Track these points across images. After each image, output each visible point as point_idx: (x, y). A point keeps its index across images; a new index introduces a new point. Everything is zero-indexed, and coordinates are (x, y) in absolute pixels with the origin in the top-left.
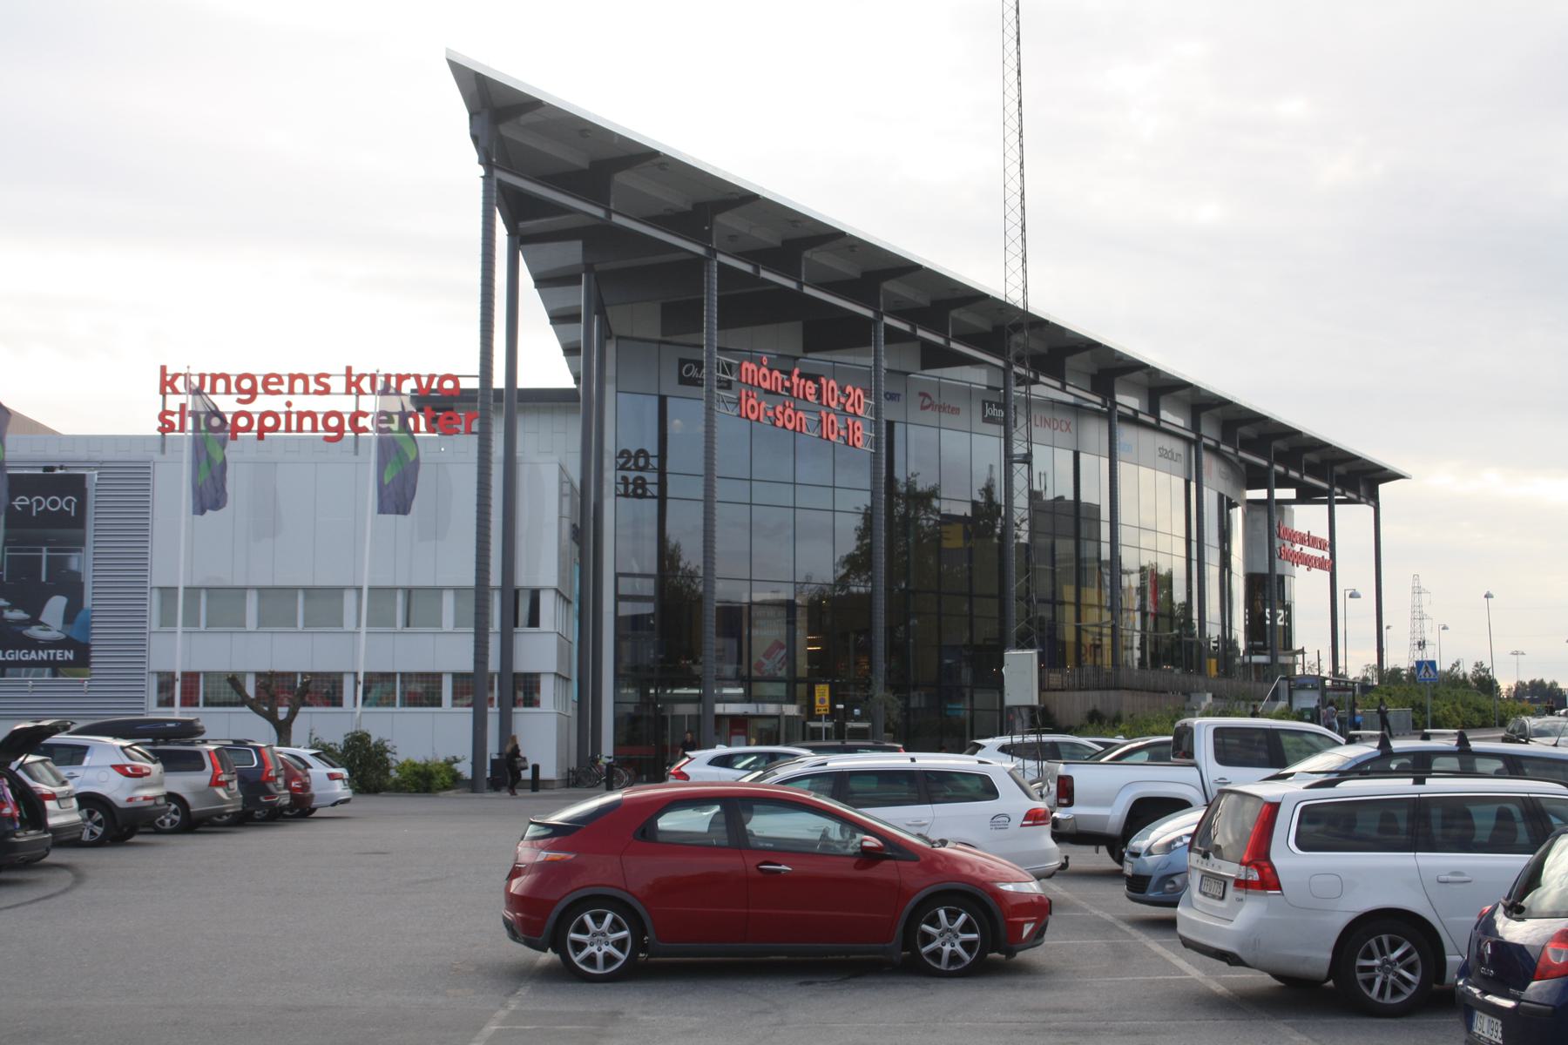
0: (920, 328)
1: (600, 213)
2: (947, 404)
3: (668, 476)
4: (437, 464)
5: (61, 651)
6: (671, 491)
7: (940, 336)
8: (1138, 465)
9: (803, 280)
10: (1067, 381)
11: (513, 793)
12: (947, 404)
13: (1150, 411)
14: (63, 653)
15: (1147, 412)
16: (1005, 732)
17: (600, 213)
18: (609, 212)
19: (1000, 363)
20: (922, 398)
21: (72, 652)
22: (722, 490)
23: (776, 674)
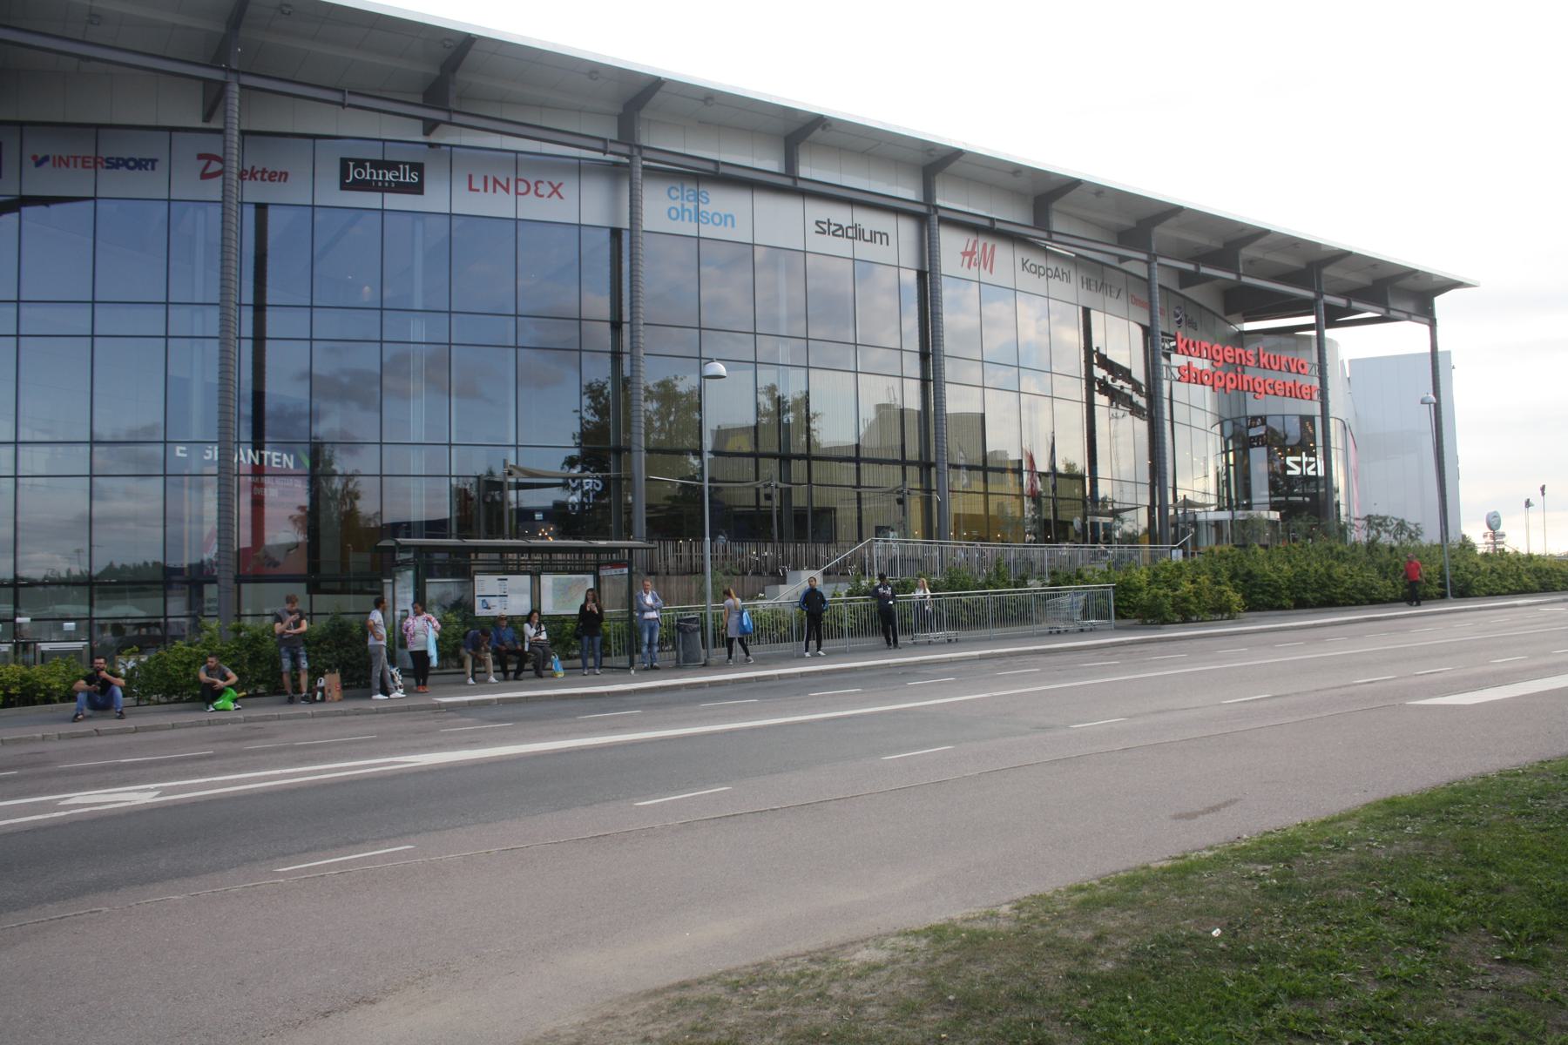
0: (1203, 266)
1: (1232, 276)
2: (259, 168)
3: (918, 376)
4: (1283, 415)
5: (279, 454)
6: (272, 328)
7: (1311, 291)
8: (451, 215)
9: (1241, 272)
10: (1392, 306)
11: (1516, 552)
12: (259, 168)
13: (1035, 223)
14: (281, 458)
15: (1116, 243)
16: (346, 691)
17: (1232, 276)
18: (1239, 275)
19: (1144, 256)
20: (204, 162)
21: (292, 457)
22: (275, 323)
23: (1115, 530)
